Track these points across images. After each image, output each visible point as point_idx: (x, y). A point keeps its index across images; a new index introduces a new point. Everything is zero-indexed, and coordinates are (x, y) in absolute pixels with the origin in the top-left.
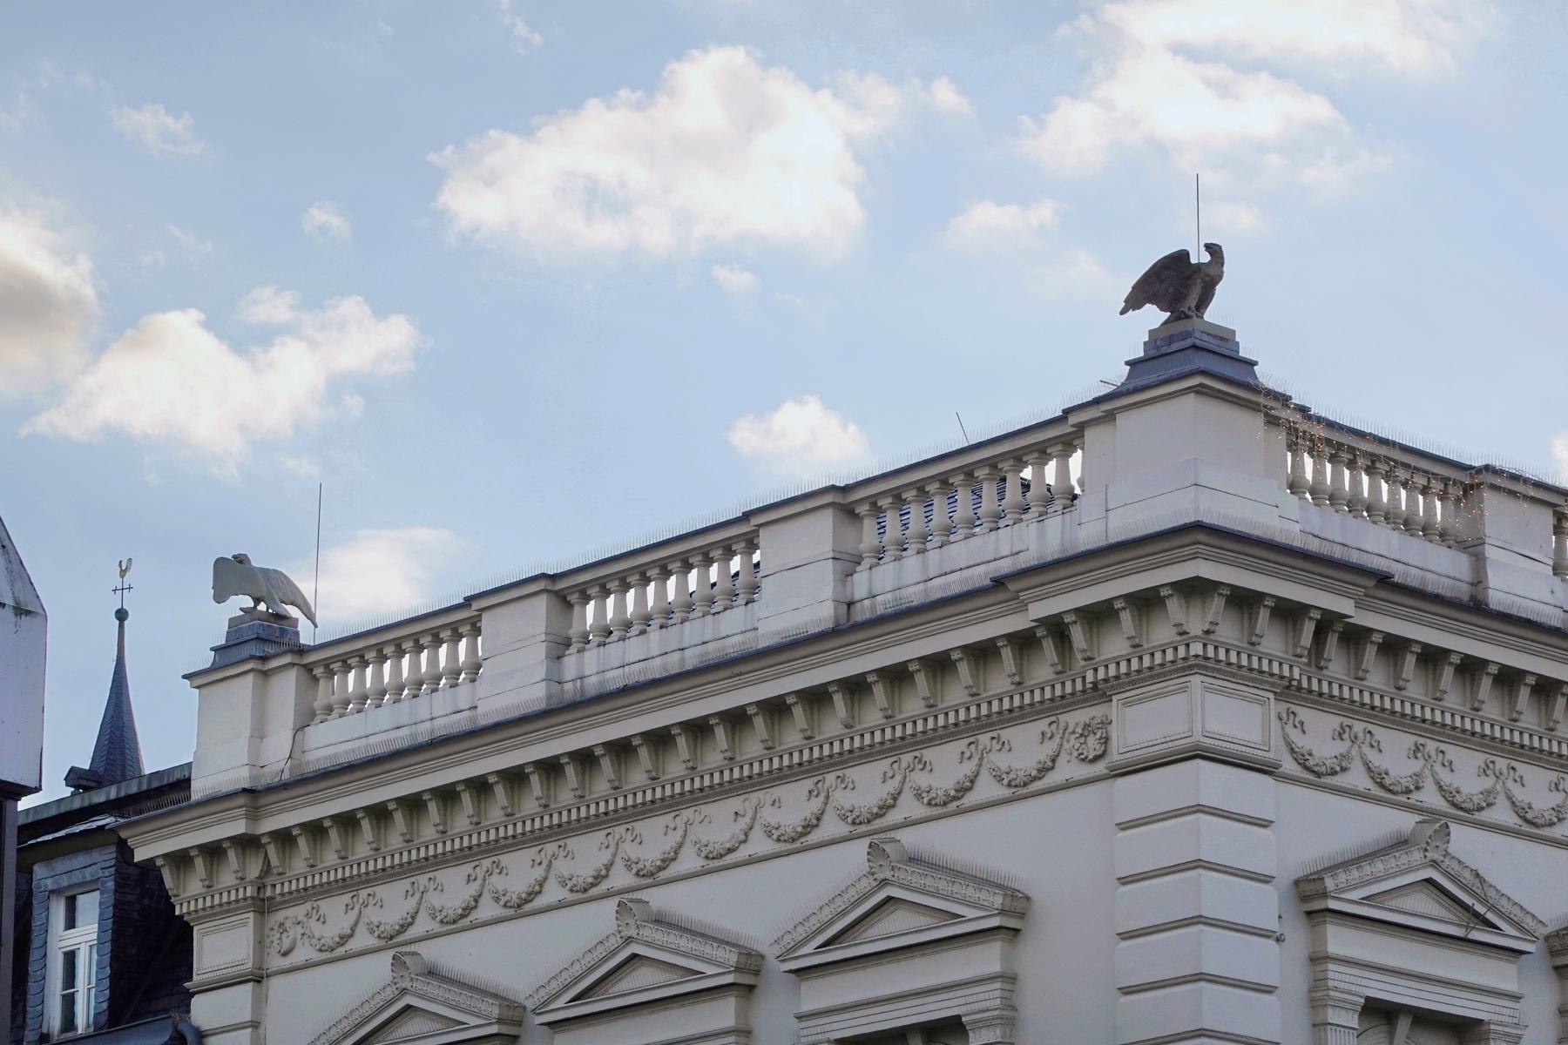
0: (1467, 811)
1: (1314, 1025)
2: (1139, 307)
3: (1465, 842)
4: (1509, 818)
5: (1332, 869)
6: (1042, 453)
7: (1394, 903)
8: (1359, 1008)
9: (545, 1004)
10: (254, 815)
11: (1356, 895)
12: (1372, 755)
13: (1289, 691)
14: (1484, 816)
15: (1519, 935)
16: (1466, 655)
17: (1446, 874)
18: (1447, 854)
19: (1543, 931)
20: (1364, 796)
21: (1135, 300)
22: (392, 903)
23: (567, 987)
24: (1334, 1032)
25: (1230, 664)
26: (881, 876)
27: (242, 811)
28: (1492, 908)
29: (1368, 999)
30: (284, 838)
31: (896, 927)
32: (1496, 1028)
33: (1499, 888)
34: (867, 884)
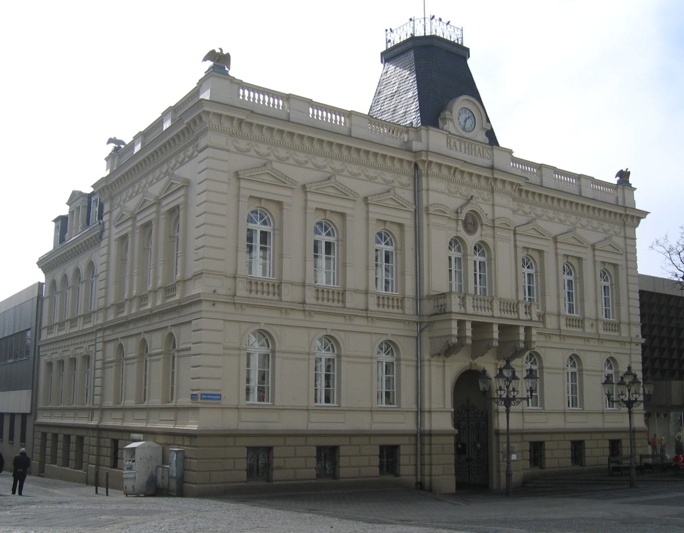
0: (538, 217)
2: (631, 184)
4: (365, 178)
5: (558, 235)
12: (547, 214)
13: (232, 135)
14: (554, 220)
19: (552, 236)
20: (547, 220)
21: (205, 59)
28: (544, 233)
31: (174, 188)
33: (290, 177)
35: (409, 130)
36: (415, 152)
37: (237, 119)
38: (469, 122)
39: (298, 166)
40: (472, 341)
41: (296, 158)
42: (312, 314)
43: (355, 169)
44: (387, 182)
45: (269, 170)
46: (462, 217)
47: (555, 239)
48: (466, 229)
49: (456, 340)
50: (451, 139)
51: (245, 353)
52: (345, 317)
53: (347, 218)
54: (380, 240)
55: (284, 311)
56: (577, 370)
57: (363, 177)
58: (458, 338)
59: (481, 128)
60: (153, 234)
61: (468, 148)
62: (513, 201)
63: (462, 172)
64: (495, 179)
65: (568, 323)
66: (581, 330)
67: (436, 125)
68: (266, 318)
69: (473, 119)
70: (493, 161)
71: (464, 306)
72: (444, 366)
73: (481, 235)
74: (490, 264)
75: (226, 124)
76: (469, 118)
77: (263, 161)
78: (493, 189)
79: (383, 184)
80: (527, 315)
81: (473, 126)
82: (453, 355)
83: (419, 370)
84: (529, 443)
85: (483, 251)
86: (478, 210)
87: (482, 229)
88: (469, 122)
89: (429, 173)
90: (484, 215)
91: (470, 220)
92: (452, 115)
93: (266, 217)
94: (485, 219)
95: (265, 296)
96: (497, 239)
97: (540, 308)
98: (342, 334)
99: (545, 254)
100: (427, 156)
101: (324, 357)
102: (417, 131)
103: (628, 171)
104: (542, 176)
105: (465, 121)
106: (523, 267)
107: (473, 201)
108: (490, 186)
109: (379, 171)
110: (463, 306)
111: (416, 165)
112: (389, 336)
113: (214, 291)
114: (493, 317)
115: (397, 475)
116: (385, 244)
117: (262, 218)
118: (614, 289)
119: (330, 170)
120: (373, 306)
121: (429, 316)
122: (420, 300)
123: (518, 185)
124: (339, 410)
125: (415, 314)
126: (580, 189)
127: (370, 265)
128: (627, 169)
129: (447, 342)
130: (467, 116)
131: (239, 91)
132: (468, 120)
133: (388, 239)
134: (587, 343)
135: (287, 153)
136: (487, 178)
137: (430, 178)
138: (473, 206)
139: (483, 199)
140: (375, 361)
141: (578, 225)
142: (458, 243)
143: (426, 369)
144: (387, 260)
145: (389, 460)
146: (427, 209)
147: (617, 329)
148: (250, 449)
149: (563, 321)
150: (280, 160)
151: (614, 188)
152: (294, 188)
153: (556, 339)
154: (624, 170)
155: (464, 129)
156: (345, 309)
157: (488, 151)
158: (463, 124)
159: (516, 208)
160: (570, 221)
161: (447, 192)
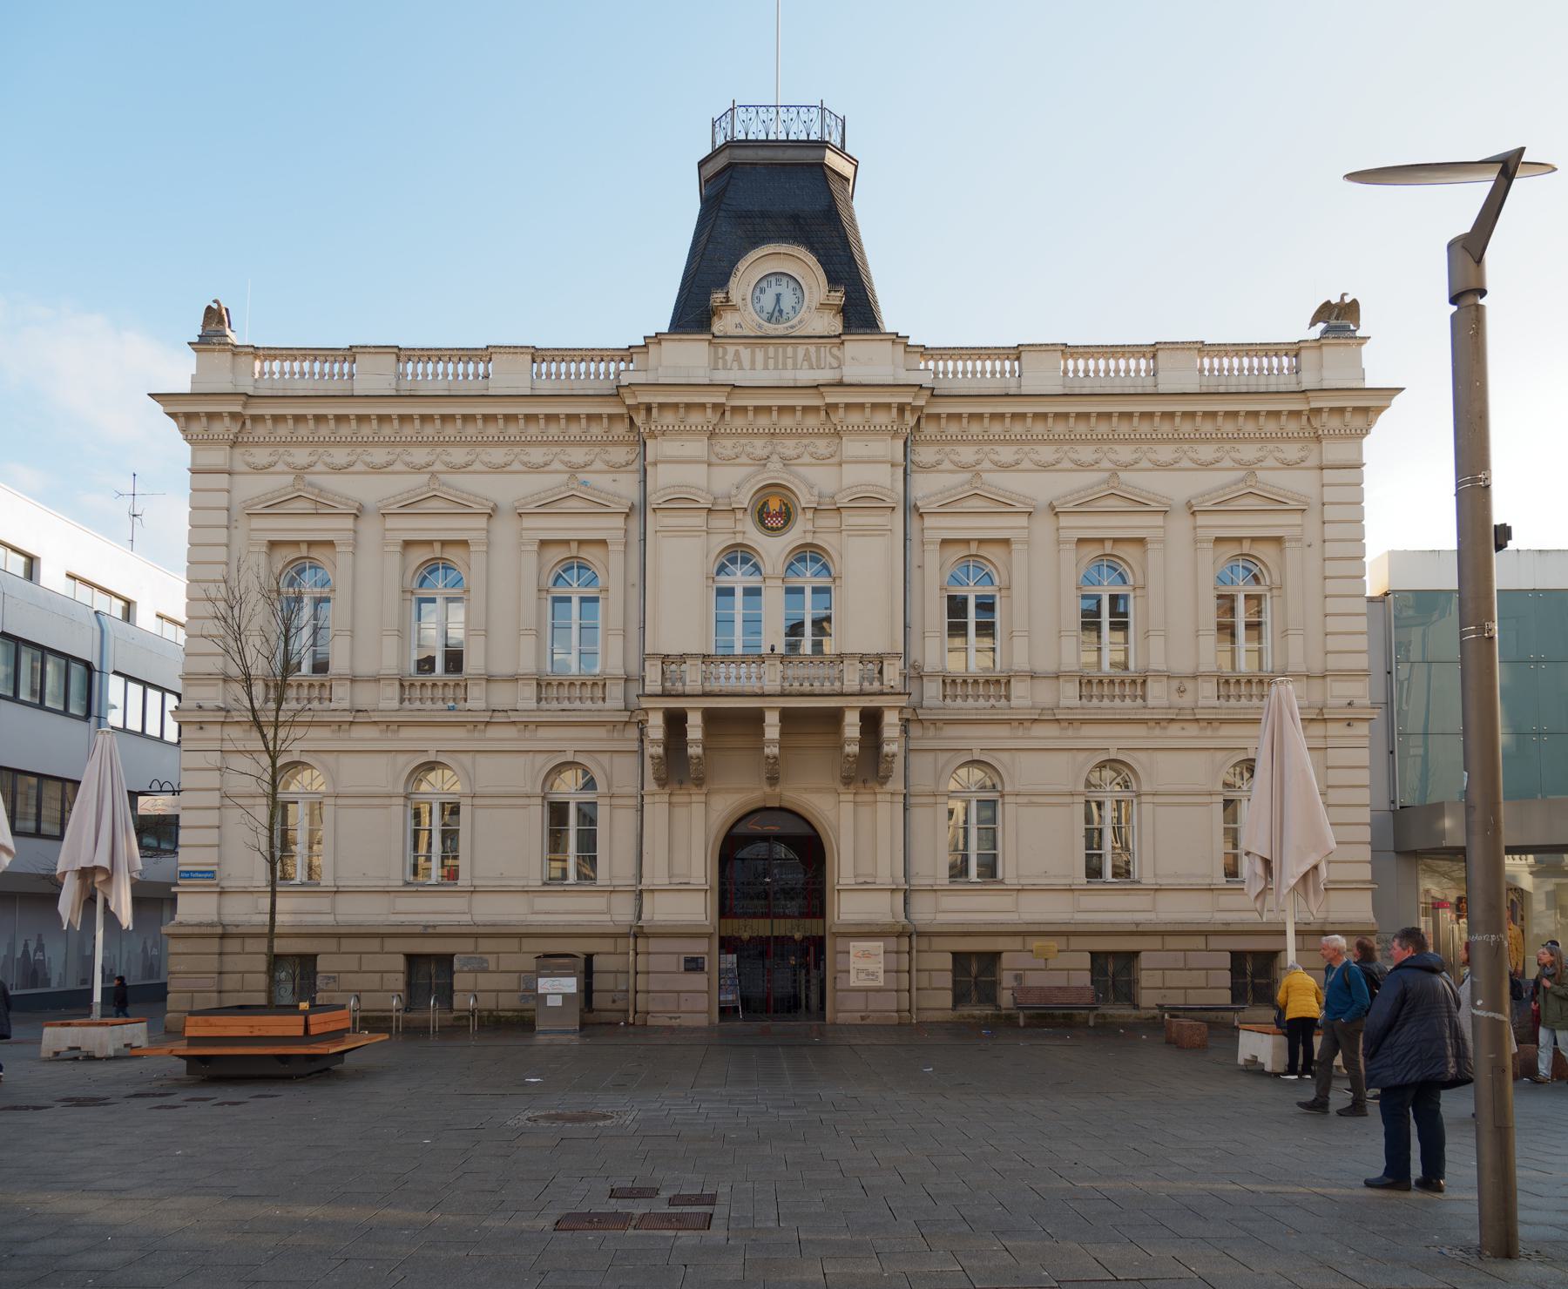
3: (1124, 476)
6: (284, 358)
9: (1063, 504)
10: (245, 406)
11: (1071, 505)
14: (1263, 464)
22: (301, 456)
23: (401, 501)
26: (297, 487)
27: (241, 402)
30: (256, 419)
34: (290, 489)
35: (1020, 352)
40: (704, 749)
42: (939, 724)
43: (340, 456)
44: (1241, 464)
46: (742, 503)
51: (1082, 799)
55: (926, 724)
68: (1114, 740)
75: (1292, 426)
79: (750, 465)
84: (951, 955)
86: (789, 481)
91: (774, 505)
103: (1347, 300)
109: (557, 449)
113: (1349, 704)
115: (1136, 1007)
119: (1111, 466)
124: (1138, 888)
128: (1343, 296)
131: (254, 364)
141: (986, 465)
145: (957, 979)
148: (957, 956)
150: (456, 469)
152: (1304, 510)
154: (1335, 300)
156: (1147, 711)
159: (765, 453)
160: (483, 463)
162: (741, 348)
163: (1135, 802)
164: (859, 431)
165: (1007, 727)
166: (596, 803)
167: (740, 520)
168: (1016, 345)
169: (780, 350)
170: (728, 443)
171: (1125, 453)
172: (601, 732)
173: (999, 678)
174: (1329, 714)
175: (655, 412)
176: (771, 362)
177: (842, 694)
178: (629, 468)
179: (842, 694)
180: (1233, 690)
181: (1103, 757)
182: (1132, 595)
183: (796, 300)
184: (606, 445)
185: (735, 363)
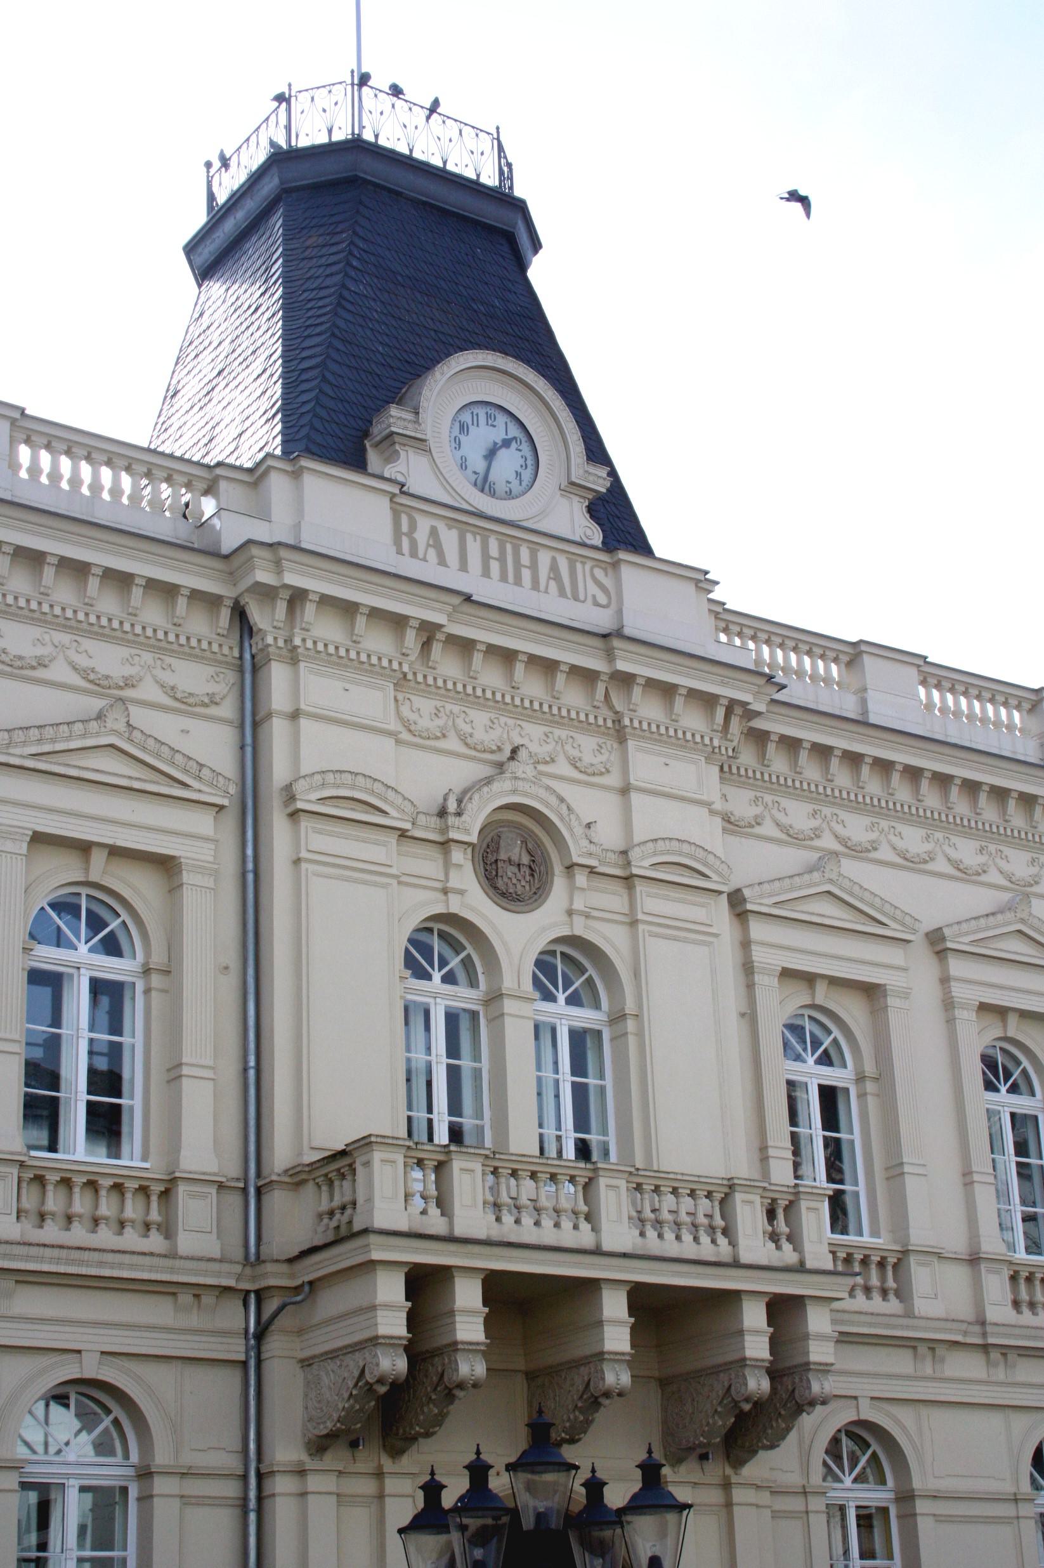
1: (947, 1022)
3: (851, 868)
7: (805, 908)
8: (28, 839)
11: (967, 939)
14: (929, 867)
15: (214, 792)
16: (106, 568)
17: (1032, 927)
18: (1031, 914)
24: (14, 860)
25: (827, 796)
29: (980, 1003)
32: (187, 861)
36: (226, 557)
37: (99, 572)
38: (508, 464)
39: (962, 880)
41: (900, 844)
42: (941, 1351)
44: (97, 684)
45: (115, 732)
46: (467, 831)
47: (938, 944)
48: (496, 888)
49: (765, 1385)
50: (419, 518)
52: (915, 1348)
53: (186, 877)
54: (799, 1048)
55: (922, 1349)
56: (891, 1495)
57: (940, 865)
58: (775, 1373)
59: (564, 483)
60: (875, 1160)
61: (502, 559)
62: (722, 779)
63: (465, 646)
64: (626, 680)
65: (1024, 1296)
66: (893, 1305)
67: (357, 462)
69: (526, 448)
70: (620, 612)
71: (443, 1202)
72: (729, 1505)
73: (570, 913)
74: (619, 1038)
76: (506, 443)
77: (98, 704)
78: (618, 721)
80: (778, 1248)
81: (527, 475)
82: (762, 1454)
83: (252, 1516)
85: (467, 963)
86: (547, 804)
87: (572, 888)
88: (508, 464)
89: (297, 641)
90: (579, 830)
91: (514, 850)
92: (417, 422)
93: (114, 925)
94: (585, 843)
95: (79, 1234)
96: (312, 867)
97: (883, 1232)
98: (905, 1415)
99: (891, 1001)
100: (278, 566)
101: (852, 1504)
102: (255, 484)
104: (865, 690)
105: (491, 455)
106: (990, 1086)
107: (522, 768)
108: (605, 712)
109: (64, 638)
110: (588, 1218)
111: (240, 615)
112: (864, 1404)
114: (736, 1264)
116: (1008, 1091)
117: (816, 1043)
118: (870, 1098)
120: (999, 1311)
121: (291, 1261)
122: (259, 1191)
123: (738, 710)
125: (238, 1254)
126: (864, 702)
127: (770, 1143)
129: (363, 1373)
130: (497, 434)
132: (503, 454)
133: (1016, 1074)
134: (1000, 1374)
135: (128, 661)
136: (588, 676)
137: (631, 744)
138: (520, 785)
139: (574, 763)
140: (817, 1504)
142: (464, 948)
143: (283, 1512)
144: (830, 1120)
146: (289, 795)
147: (891, 1283)
149: (996, 1287)
151: (1026, 706)
153: (968, 1366)
155: (484, 484)
157: (598, 573)
158: (480, 465)
161: (393, 725)
162: (441, 526)
163: (133, 1493)
164: (655, 736)
165: (166, 1303)
166: (64, 1484)
167: (583, 889)
168: (854, 640)
169: (509, 547)
170: (426, 705)
171: (857, 827)
172: (159, 1311)
173: (68, 1175)
174: (998, 1335)
175: (310, 609)
176: (495, 566)
177: (451, 1239)
178: (213, 711)
179: (451, 1239)
180: (54, 1201)
181: (70, 1371)
182: (140, 987)
183: (522, 461)
184: (172, 653)
185: (552, 584)
